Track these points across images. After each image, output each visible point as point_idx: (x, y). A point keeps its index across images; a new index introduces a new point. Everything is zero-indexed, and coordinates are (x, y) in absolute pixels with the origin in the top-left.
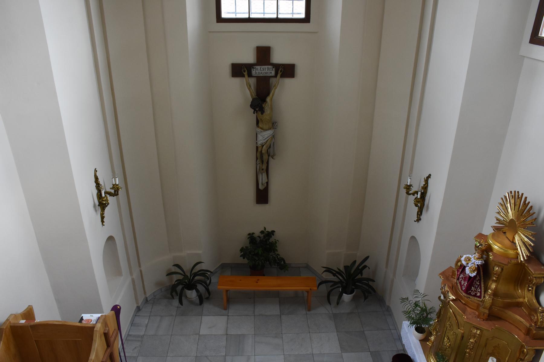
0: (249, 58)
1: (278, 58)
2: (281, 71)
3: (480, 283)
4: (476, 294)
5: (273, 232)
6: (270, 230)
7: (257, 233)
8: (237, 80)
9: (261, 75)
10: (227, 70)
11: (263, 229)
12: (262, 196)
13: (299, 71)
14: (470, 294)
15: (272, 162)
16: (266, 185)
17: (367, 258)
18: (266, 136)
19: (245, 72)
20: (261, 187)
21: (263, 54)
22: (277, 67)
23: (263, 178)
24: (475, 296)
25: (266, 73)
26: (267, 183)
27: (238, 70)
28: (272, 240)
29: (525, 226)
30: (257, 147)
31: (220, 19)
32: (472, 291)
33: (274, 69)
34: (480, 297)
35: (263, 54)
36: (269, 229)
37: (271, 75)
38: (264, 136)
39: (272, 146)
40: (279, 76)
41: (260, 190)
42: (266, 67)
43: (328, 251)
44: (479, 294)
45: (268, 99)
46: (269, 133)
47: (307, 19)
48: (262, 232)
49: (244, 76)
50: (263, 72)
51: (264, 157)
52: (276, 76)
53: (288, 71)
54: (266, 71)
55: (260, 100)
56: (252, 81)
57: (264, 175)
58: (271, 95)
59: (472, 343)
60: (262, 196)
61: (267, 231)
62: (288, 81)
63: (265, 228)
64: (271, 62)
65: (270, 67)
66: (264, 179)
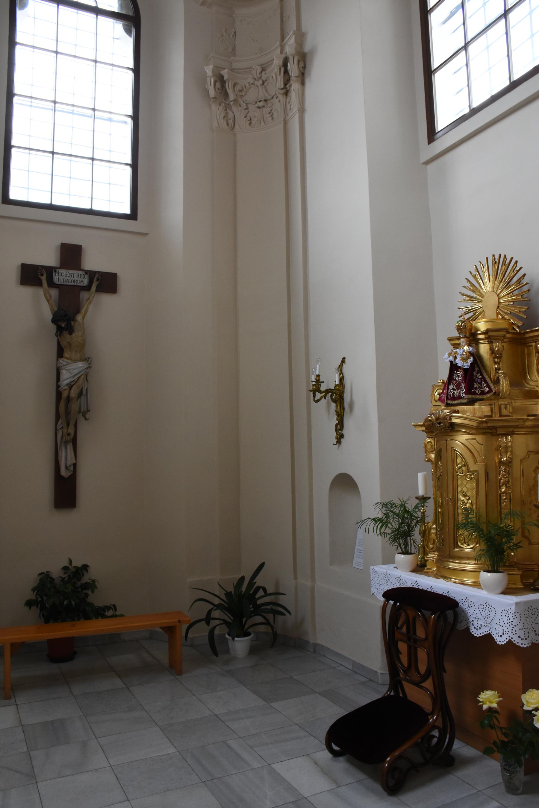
0: (48, 258)
1: (93, 261)
2: (98, 280)
3: (482, 375)
4: (483, 391)
5: (85, 567)
6: (79, 565)
7: (56, 572)
8: (28, 291)
9: (67, 283)
10: (14, 274)
11: (66, 564)
12: (65, 492)
13: (123, 284)
14: (475, 393)
15: (83, 426)
16: (72, 468)
17: (262, 566)
18: (76, 372)
19: (42, 275)
20: (64, 473)
21: (71, 254)
22: (92, 275)
23: (66, 456)
24: (483, 393)
25: (75, 281)
26: (75, 465)
27: (30, 275)
28: (85, 579)
29: (416, 641)
30: (59, 394)
31: (6, 200)
32: (476, 388)
33: (86, 276)
34: (490, 390)
35: (71, 254)
36: (78, 563)
37: (82, 284)
38: (72, 370)
39: (84, 392)
40: (94, 288)
41: (62, 477)
42: (75, 272)
43: (193, 575)
44: (487, 389)
45: (79, 318)
46: (81, 365)
47: (133, 216)
48: (65, 568)
49: (39, 284)
50: (70, 279)
51: (69, 409)
52: (88, 288)
53: (107, 283)
54: (75, 278)
55: (65, 320)
56: (54, 293)
57: (70, 447)
58: (83, 311)
59: (506, 506)
60: (65, 492)
61: (75, 567)
62: (106, 299)
63: (71, 561)
64: (82, 268)
65: (80, 272)
66: (69, 457)
